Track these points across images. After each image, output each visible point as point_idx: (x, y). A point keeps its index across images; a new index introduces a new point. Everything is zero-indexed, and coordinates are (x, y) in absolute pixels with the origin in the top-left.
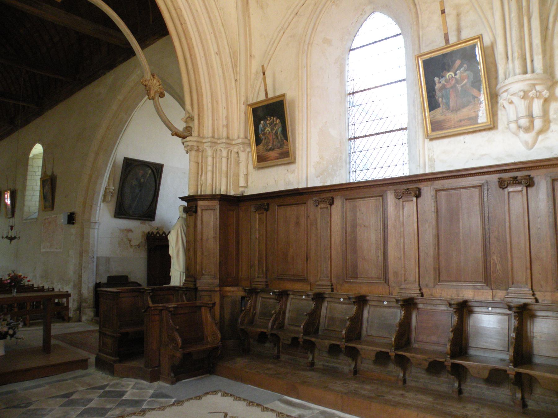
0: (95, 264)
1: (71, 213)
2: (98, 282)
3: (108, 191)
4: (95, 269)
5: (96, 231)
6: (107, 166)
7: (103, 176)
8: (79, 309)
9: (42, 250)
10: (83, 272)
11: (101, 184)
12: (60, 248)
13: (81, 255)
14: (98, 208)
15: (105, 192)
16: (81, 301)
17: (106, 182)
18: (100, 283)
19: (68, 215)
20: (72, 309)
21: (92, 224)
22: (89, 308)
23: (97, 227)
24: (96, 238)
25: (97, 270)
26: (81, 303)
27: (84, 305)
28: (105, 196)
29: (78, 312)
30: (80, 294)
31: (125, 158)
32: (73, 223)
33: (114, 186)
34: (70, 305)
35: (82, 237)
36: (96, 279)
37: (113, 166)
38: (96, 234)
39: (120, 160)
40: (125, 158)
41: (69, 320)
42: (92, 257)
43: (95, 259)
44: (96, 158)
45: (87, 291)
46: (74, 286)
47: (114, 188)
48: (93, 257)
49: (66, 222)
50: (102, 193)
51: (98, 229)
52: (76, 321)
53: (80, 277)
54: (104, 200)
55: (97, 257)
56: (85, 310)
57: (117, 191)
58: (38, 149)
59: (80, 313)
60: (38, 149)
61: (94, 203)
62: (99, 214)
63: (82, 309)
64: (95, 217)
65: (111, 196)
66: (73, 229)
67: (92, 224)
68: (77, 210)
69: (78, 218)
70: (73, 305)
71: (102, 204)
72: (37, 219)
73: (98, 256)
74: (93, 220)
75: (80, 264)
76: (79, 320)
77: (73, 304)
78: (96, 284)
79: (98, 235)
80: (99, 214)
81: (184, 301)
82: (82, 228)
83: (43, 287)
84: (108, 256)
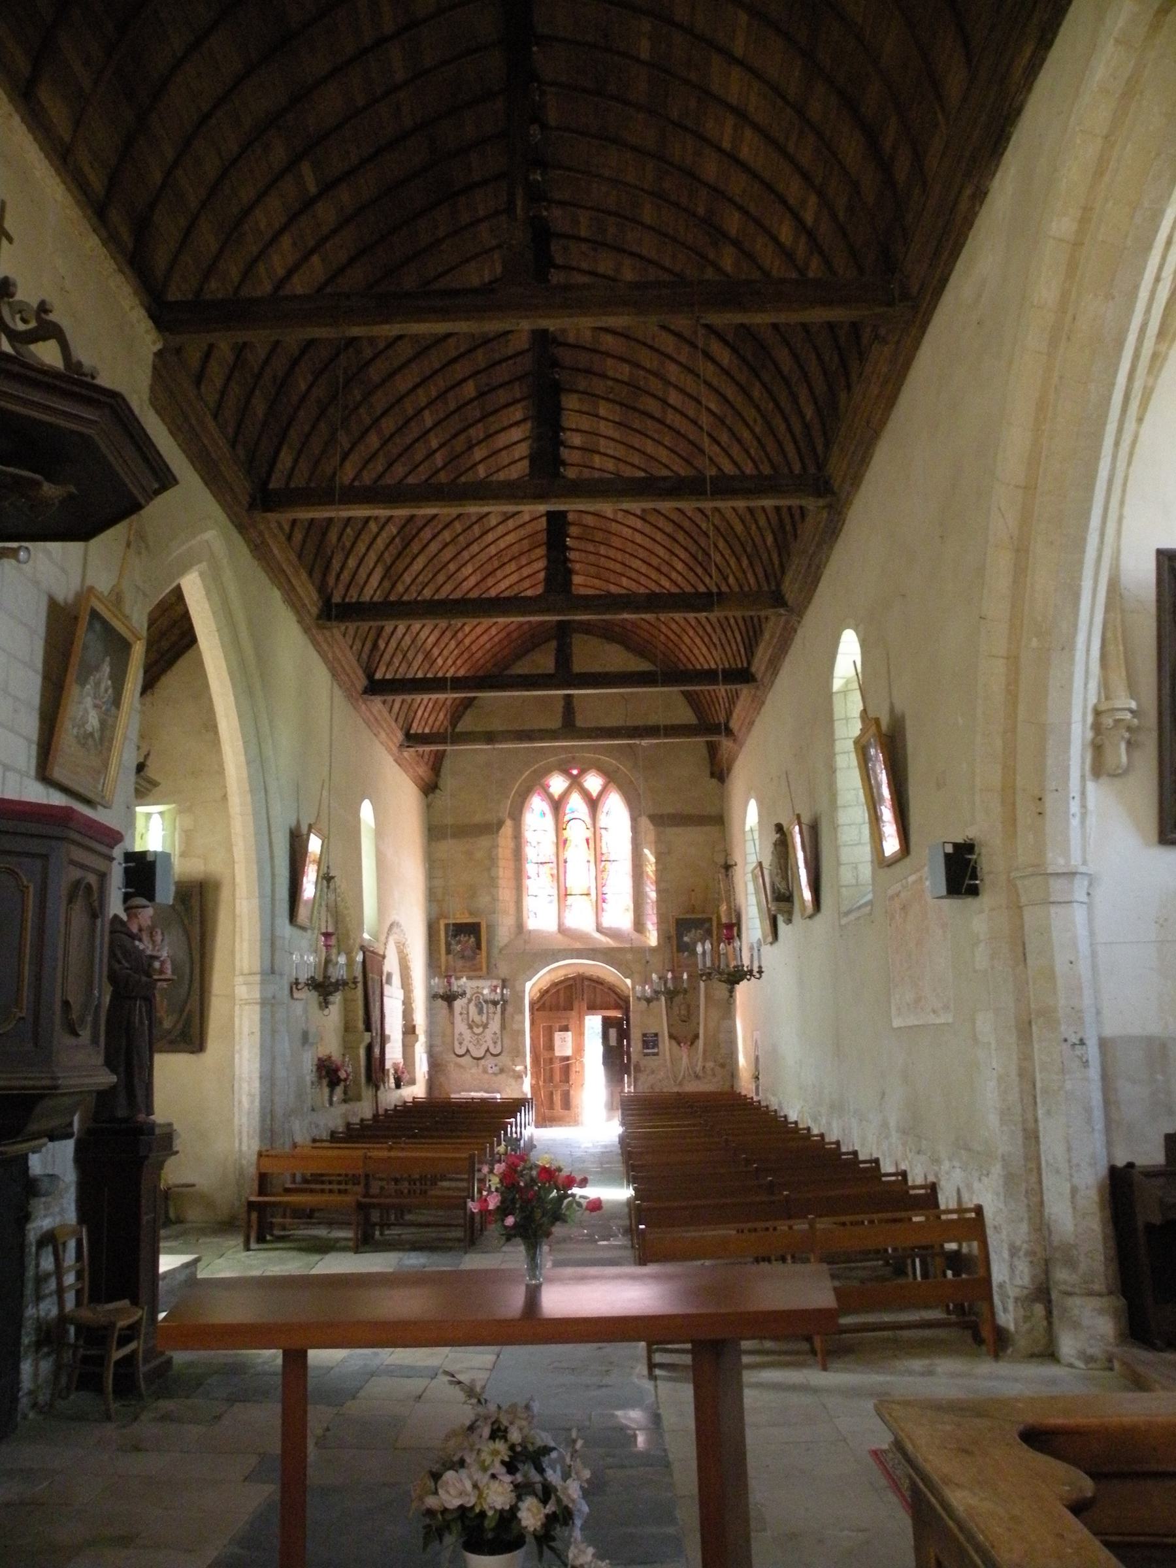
0: (1094, 1072)
1: (956, 846)
2: (1120, 1163)
3: (1108, 721)
4: (1096, 1097)
5: (1079, 914)
6: (1077, 597)
7: (1068, 646)
8: (1042, 1293)
9: (897, 1023)
10: (1040, 1113)
11: (1066, 688)
12: (946, 1008)
13: (1024, 1031)
14: (1075, 807)
15: (1097, 727)
16: (1047, 1257)
17: (1093, 685)
18: (1131, 1165)
19: (947, 856)
20: (1012, 1292)
21: (1056, 885)
22: (1091, 1294)
23: (1080, 895)
24: (1084, 947)
25: (1107, 1103)
26: (1047, 1262)
27: (1062, 1275)
28: (1097, 749)
29: (1039, 1309)
30: (1040, 1225)
31: (1160, 552)
32: (974, 891)
33: (1133, 695)
34: (999, 1273)
35: (1019, 947)
36: (1109, 1144)
37: (1108, 608)
38: (1082, 932)
39: (1142, 575)
40: (1160, 552)
41: (998, 1343)
42: (1074, 1039)
43: (1092, 1051)
44: (1020, 571)
45: (1073, 1207)
46: (1010, 1179)
47: (1137, 701)
48: (1082, 1042)
49: (942, 889)
50: (1079, 732)
51: (1090, 906)
52: (1032, 1356)
53: (1032, 1137)
54: (1098, 769)
55: (1103, 1044)
56: (1070, 1302)
57: (1152, 720)
58: (849, 648)
59: (1049, 1313)
60: (849, 648)
61: (1051, 785)
62: (1084, 837)
63: (1054, 1295)
64: (1066, 853)
65: (1129, 743)
66: (978, 916)
67: (1056, 885)
68: (979, 825)
69: (990, 863)
70: (1008, 1274)
71: (1091, 786)
72: (870, 903)
73: (1108, 1032)
74: (1055, 862)
75: (1026, 1075)
76: (1050, 1354)
77: (1012, 1268)
78: (1113, 1171)
79: (1092, 933)
80: (1084, 837)
81: (144, 1364)
82: (1016, 908)
83: (933, 1188)
84: (1154, 1028)
